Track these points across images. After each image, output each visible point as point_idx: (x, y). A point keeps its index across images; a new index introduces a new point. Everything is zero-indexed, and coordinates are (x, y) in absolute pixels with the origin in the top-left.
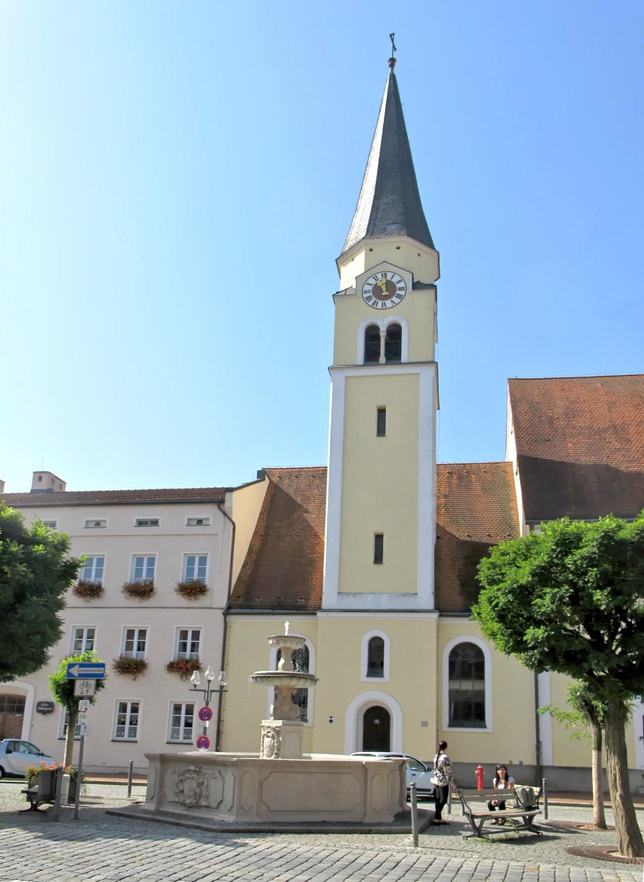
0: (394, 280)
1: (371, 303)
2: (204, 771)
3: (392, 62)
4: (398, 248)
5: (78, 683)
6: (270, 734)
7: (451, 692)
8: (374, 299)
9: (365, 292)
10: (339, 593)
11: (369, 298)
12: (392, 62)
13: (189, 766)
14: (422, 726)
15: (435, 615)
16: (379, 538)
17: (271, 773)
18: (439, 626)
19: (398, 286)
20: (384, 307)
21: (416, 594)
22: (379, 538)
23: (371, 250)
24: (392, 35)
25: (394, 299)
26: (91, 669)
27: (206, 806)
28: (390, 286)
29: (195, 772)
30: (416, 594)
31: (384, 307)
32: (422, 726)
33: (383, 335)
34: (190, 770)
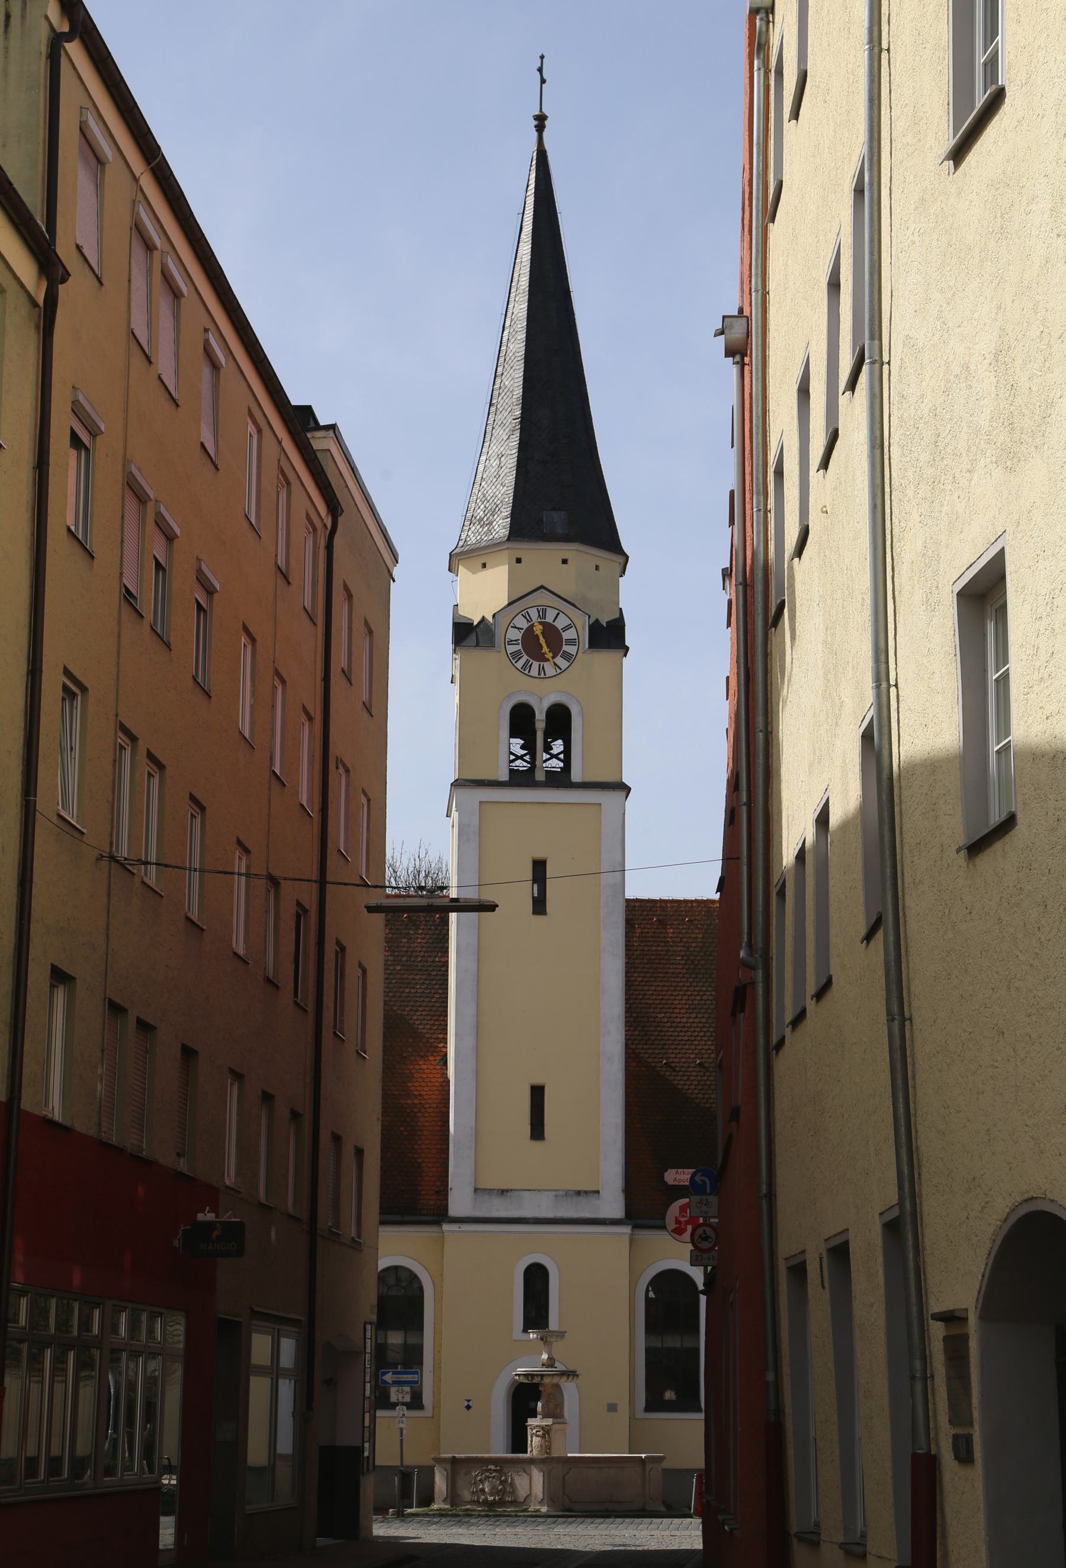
0: (560, 624)
1: (520, 664)
2: (506, 1470)
3: (541, 121)
4: (565, 562)
5: (393, 1390)
6: (540, 1433)
7: (649, 1351)
8: (525, 658)
9: (511, 642)
10: (476, 1190)
11: (516, 656)
12: (541, 121)
13: (487, 1467)
14: (609, 1411)
15: (627, 1230)
16: (537, 1093)
17: (570, 1469)
18: (632, 1242)
19: (566, 635)
20: (542, 675)
21: (598, 1192)
22: (537, 1093)
23: (519, 561)
24: (542, 57)
25: (559, 660)
26: (406, 1376)
27: (511, 1502)
28: (552, 635)
29: (495, 1471)
30: (598, 1192)
31: (542, 675)
32: (609, 1411)
33: (540, 717)
34: (490, 1470)
